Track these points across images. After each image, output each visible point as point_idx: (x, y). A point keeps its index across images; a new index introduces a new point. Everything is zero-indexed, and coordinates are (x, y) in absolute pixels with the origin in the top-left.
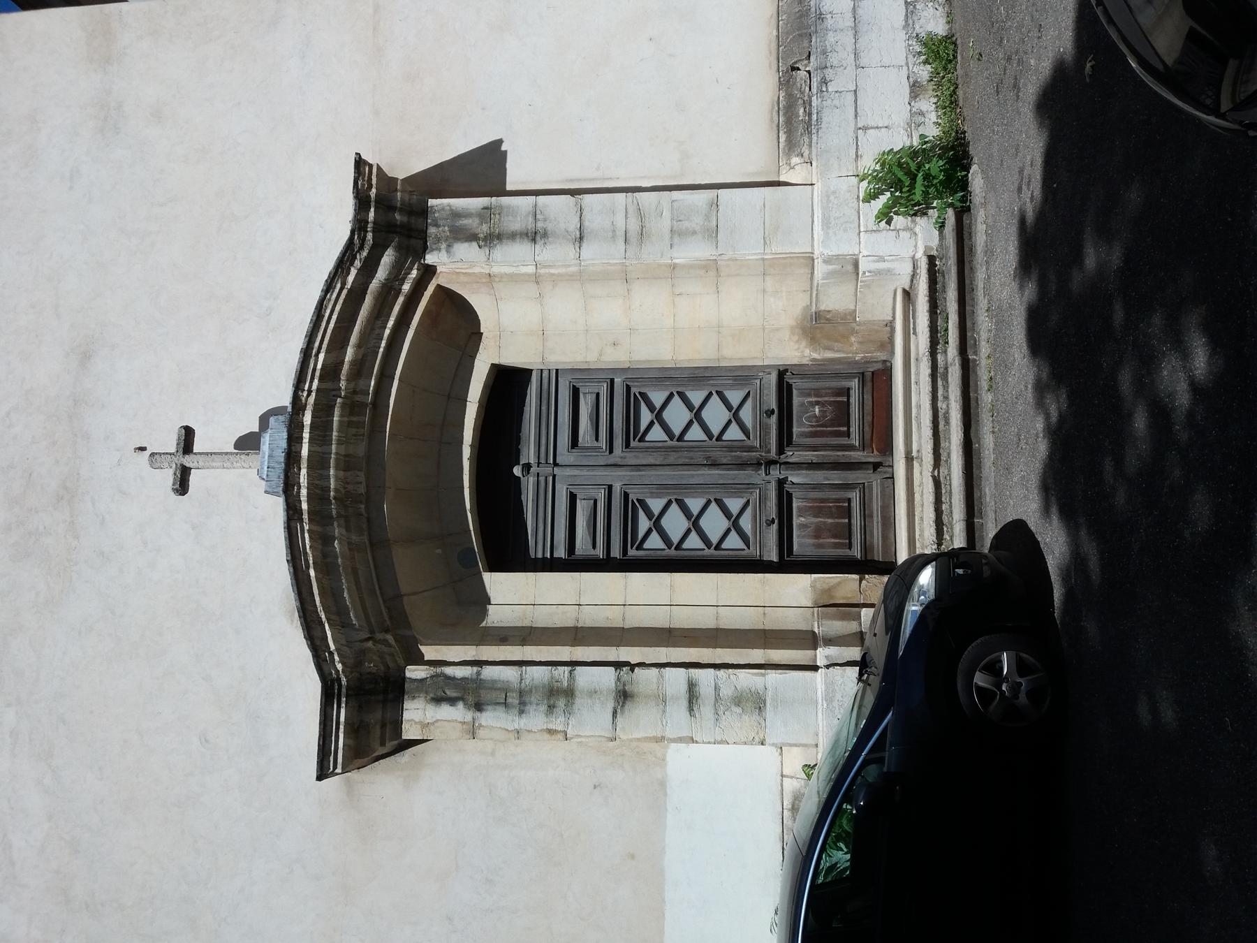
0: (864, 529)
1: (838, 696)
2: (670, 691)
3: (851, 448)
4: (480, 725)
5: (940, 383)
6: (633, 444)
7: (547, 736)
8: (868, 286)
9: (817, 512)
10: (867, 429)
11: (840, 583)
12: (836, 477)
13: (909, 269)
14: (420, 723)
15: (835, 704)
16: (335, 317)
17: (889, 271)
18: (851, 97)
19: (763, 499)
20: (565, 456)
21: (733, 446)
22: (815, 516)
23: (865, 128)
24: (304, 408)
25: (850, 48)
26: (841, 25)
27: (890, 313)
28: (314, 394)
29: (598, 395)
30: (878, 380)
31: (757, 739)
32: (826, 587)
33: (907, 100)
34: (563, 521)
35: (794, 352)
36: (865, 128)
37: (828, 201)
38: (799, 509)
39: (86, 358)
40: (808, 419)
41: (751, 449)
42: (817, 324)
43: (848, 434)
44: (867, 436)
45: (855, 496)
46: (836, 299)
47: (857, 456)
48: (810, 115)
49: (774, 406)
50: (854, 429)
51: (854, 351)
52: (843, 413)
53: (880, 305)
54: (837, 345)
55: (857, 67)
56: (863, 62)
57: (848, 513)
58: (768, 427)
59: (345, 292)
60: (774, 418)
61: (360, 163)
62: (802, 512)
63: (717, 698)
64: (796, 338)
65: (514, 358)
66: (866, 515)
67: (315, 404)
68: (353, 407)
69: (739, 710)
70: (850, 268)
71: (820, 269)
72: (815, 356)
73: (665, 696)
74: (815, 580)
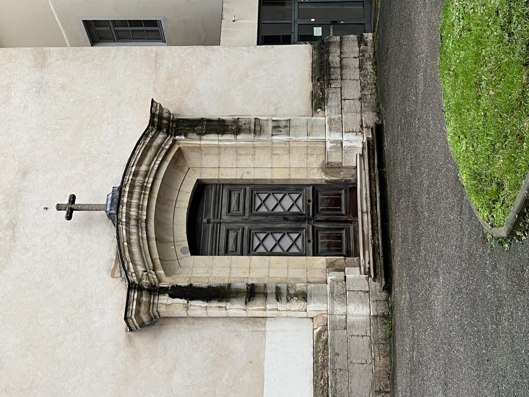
0: (348, 244)
1: (335, 292)
2: (269, 291)
3: (342, 215)
4: (191, 305)
5: (373, 182)
6: (253, 212)
7: (218, 309)
8: (346, 153)
9: (328, 237)
10: (348, 207)
11: (337, 260)
12: (335, 226)
13: (362, 146)
14: (166, 304)
15: (334, 295)
16: (140, 154)
17: (354, 146)
18: (339, 89)
19: (307, 232)
20: (225, 217)
21: (294, 214)
22: (328, 239)
23: (345, 100)
24: (125, 186)
25: (339, 73)
26: (336, 66)
27: (355, 163)
28: (130, 181)
29: (239, 194)
30: (352, 189)
31: (303, 309)
32: (332, 261)
33: (360, 90)
34: (224, 240)
35: (318, 176)
36: (345, 100)
37: (331, 122)
38: (321, 237)
39: (25, 174)
40: (325, 204)
41: (303, 214)
42: (328, 167)
43: (340, 210)
44: (348, 211)
45: (344, 232)
46: (335, 158)
47: (344, 218)
48: (324, 95)
49: (311, 199)
50: (343, 208)
51: (342, 176)
52: (338, 202)
53: (352, 160)
54: (335, 175)
55: (342, 79)
56: (344, 77)
57: (340, 238)
58: (309, 206)
59: (144, 146)
60: (311, 204)
61: (153, 101)
62: (322, 238)
63: (288, 294)
64: (320, 172)
65: (209, 174)
66: (348, 239)
67: (130, 184)
68: (143, 187)
69: (296, 298)
70: (339, 145)
71: (328, 145)
72: (327, 178)
73: (267, 293)
74: (327, 259)
